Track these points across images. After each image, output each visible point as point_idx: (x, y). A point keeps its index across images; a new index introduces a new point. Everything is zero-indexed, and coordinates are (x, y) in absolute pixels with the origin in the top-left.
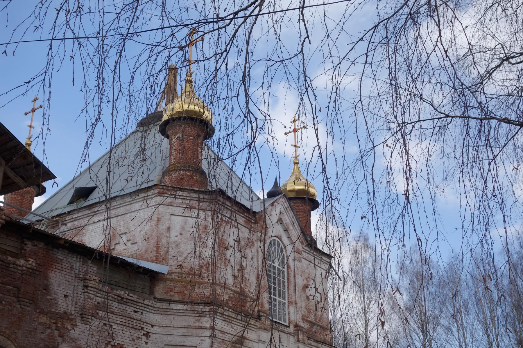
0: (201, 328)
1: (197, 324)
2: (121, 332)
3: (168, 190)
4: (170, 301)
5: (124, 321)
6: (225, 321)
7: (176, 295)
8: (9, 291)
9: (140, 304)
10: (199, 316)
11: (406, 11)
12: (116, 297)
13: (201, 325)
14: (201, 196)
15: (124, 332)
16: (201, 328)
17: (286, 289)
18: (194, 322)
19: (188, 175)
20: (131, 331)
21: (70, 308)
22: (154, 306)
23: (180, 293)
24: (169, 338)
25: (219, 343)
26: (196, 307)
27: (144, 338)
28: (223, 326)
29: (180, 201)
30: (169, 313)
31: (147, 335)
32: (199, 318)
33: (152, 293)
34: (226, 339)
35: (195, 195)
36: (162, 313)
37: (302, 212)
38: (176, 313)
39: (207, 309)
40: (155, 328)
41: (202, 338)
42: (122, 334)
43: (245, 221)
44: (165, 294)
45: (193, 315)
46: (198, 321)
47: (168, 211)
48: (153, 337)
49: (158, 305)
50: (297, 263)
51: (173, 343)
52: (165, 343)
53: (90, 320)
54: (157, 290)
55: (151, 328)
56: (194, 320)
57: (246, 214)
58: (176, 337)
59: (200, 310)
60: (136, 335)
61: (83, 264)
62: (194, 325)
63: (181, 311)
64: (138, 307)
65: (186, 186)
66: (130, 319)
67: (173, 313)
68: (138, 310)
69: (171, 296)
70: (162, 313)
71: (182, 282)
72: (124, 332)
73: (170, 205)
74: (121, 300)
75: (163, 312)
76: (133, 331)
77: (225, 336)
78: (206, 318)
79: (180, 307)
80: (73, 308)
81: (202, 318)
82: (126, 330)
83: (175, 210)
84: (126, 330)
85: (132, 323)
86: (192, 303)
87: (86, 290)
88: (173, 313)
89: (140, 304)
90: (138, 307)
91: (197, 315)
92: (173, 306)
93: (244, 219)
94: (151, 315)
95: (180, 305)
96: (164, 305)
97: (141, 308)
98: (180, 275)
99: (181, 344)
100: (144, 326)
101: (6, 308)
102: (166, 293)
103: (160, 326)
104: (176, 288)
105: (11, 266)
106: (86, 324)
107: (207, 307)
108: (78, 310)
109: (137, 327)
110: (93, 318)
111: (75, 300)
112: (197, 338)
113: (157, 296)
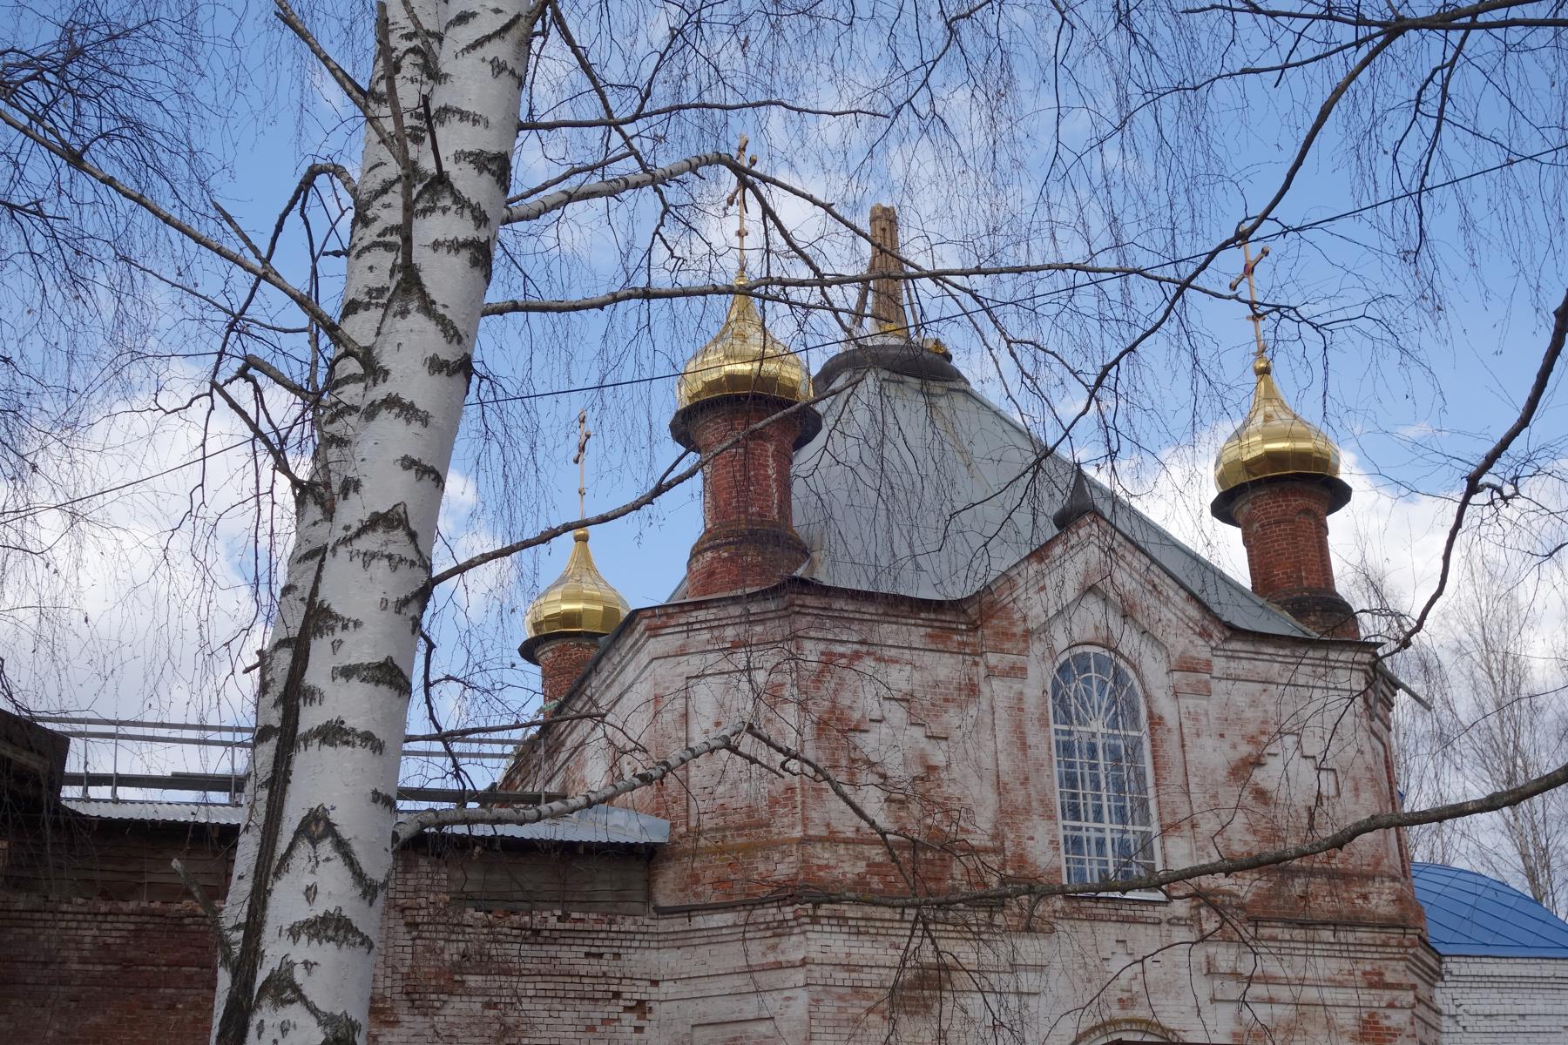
0: (779, 966)
1: (771, 958)
2: (545, 1014)
3: (669, 616)
4: (688, 911)
5: (552, 986)
6: (859, 933)
7: (709, 890)
8: (189, 978)
9: (602, 935)
10: (774, 936)
11: (543, 90)
12: (515, 932)
13: (781, 958)
14: (754, 608)
15: (555, 1014)
16: (779, 966)
17: (1151, 793)
18: (764, 954)
19: (725, 560)
20: (580, 1008)
21: (380, 985)
22: (651, 929)
23: (719, 883)
24: (702, 1006)
25: (841, 998)
26: (759, 912)
27: (630, 1019)
28: (854, 950)
29: (706, 635)
30: (696, 941)
31: (641, 1008)
32: (776, 940)
33: (649, 897)
34: (867, 984)
35: (735, 610)
36: (678, 943)
37: (1278, 523)
38: (713, 937)
39: (788, 912)
40: (664, 987)
41: (786, 993)
42: (551, 1021)
43: (928, 635)
44: (681, 895)
45: (759, 934)
46: (774, 948)
47: (679, 670)
48: (660, 1011)
49: (664, 925)
50: (1189, 702)
51: (711, 1019)
52: (692, 1022)
53: (437, 1004)
54: (661, 886)
55: (654, 990)
56: (762, 948)
57: (923, 615)
58: (719, 1001)
59: (769, 918)
60: (599, 1015)
61: (405, 872)
62: (764, 961)
63: (724, 931)
64: (598, 943)
65: (721, 590)
66: (568, 979)
67: (705, 940)
68: (602, 950)
69: (696, 895)
70: (678, 943)
71: (722, 853)
72: (555, 1014)
73: (682, 652)
74: (535, 935)
75: (681, 941)
76: (586, 1006)
77: (862, 976)
78: (793, 938)
79: (718, 919)
80: (388, 983)
81: (785, 939)
82: (561, 1007)
83: (694, 664)
84: (561, 1007)
85: (579, 987)
86: (751, 904)
87: (415, 933)
88: (705, 940)
89: (602, 935)
90: (598, 943)
91: (769, 933)
92: (700, 921)
93: (922, 631)
94: (652, 955)
95: (717, 917)
96: (678, 924)
97: (607, 943)
98: (719, 835)
99: (734, 1017)
100: (621, 989)
101: (190, 1017)
102: (682, 890)
103: (675, 980)
104: (709, 873)
105: (187, 921)
106: (426, 1015)
107: (788, 909)
108: (400, 983)
109: (598, 995)
110: (443, 997)
111: (390, 962)
112: (774, 994)
113: (663, 901)
